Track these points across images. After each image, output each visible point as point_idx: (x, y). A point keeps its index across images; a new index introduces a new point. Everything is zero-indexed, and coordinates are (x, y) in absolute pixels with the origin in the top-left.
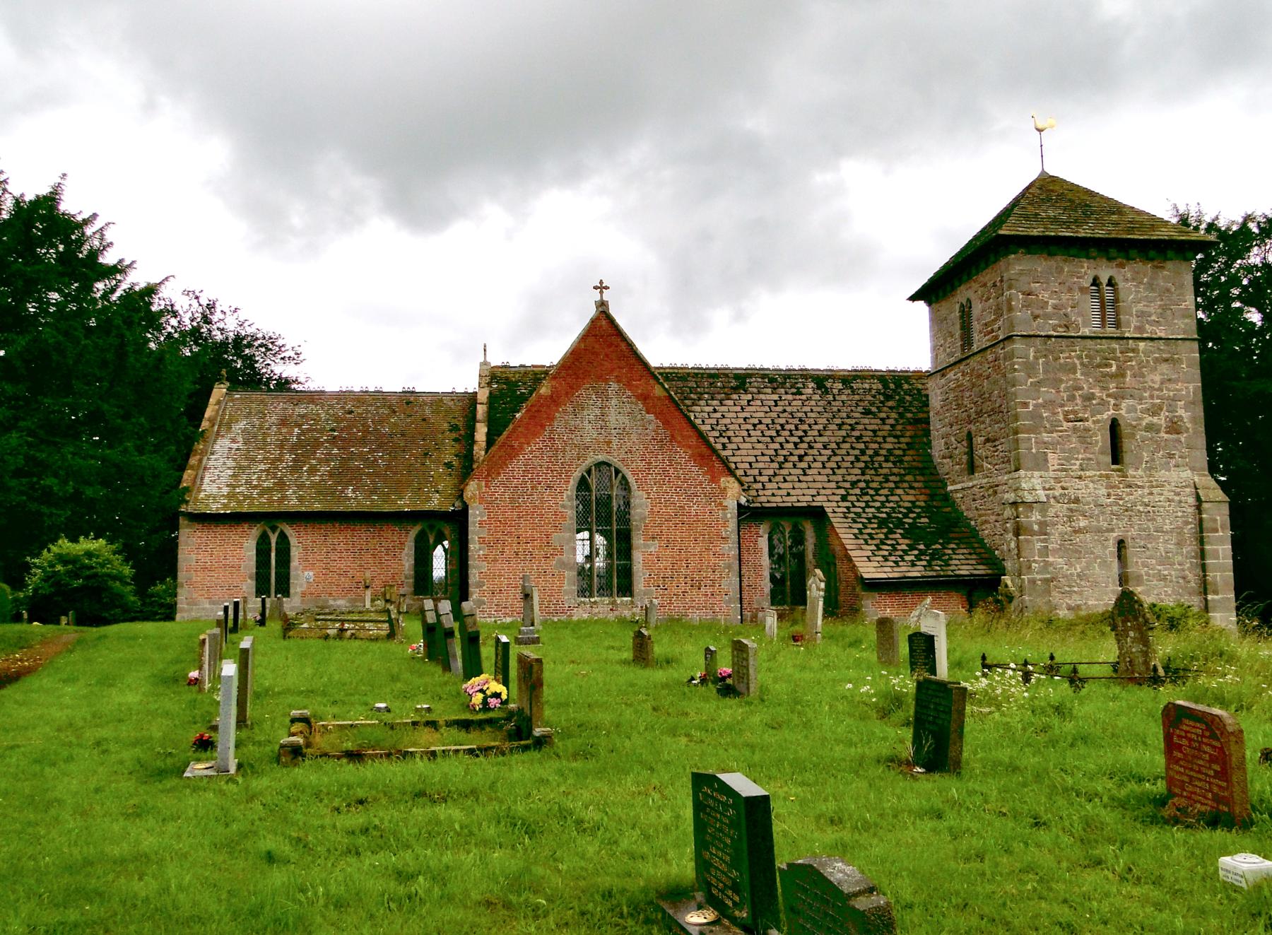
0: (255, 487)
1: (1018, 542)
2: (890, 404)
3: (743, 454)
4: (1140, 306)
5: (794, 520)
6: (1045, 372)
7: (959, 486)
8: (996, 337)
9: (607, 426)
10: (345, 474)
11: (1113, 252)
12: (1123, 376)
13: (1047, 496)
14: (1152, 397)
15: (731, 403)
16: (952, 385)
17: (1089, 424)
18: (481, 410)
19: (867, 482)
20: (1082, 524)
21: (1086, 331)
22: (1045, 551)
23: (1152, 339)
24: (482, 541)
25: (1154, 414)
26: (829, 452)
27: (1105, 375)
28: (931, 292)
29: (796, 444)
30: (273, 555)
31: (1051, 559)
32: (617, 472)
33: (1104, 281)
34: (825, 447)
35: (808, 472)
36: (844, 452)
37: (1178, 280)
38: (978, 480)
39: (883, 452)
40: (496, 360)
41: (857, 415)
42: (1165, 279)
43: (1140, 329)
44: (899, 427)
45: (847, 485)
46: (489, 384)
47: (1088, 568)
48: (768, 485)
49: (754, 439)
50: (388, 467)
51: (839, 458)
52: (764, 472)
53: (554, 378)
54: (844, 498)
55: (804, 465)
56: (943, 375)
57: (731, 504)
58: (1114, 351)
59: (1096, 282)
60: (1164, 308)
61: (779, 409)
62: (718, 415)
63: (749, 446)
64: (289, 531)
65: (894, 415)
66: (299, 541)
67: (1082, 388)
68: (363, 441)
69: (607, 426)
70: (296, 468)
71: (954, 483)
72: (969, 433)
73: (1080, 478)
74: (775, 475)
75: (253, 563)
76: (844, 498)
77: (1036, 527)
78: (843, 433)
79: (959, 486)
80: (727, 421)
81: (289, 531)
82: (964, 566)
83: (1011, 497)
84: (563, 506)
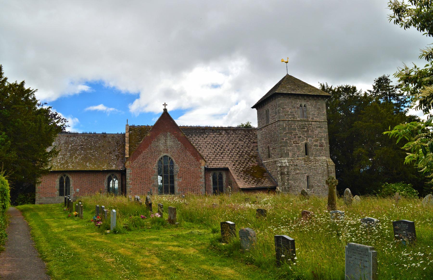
0: (59, 163)
1: (281, 177)
2: (247, 137)
3: (205, 152)
4: (312, 112)
5: (220, 171)
6: (288, 130)
7: (265, 162)
8: (275, 120)
9: (166, 145)
10: (86, 159)
11: (305, 98)
12: (308, 131)
13: (289, 164)
14: (316, 137)
15: (201, 137)
16: (264, 133)
17: (300, 144)
18: (127, 139)
19: (240, 160)
20: (298, 172)
21: (299, 119)
22: (288, 180)
23: (315, 121)
24: (130, 179)
25: (316, 142)
26: (229, 152)
27: (304, 131)
28: (257, 106)
29: (220, 149)
30: (65, 183)
31: (290, 182)
32: (170, 158)
33: (303, 105)
34: (228, 150)
35: (224, 157)
36: (233, 152)
37: (322, 104)
38: (271, 160)
39: (245, 152)
40: (130, 124)
41: (237, 141)
42: (319, 105)
43: (313, 119)
44: (249, 144)
45: (235, 161)
46: (129, 131)
47: (299, 184)
48: (212, 162)
49: (208, 148)
50: (99, 157)
51: (232, 154)
52: (211, 158)
53: (151, 131)
54: (234, 165)
55: (222, 155)
56: (261, 130)
57: (203, 168)
58: (306, 124)
59: (301, 106)
60: (319, 113)
61: (215, 139)
62: (198, 141)
63: (207, 150)
64: (70, 176)
65: (248, 141)
66: (72, 180)
67: (297, 135)
68: (91, 149)
69: (166, 145)
70: (71, 157)
71: (264, 160)
72: (268, 147)
73: (297, 159)
74: (214, 158)
75: (59, 186)
76: (234, 165)
77: (286, 173)
78: (233, 146)
79: (265, 162)
80: (200, 143)
81: (70, 176)
82: (267, 184)
83: (279, 165)
84: (154, 169)
